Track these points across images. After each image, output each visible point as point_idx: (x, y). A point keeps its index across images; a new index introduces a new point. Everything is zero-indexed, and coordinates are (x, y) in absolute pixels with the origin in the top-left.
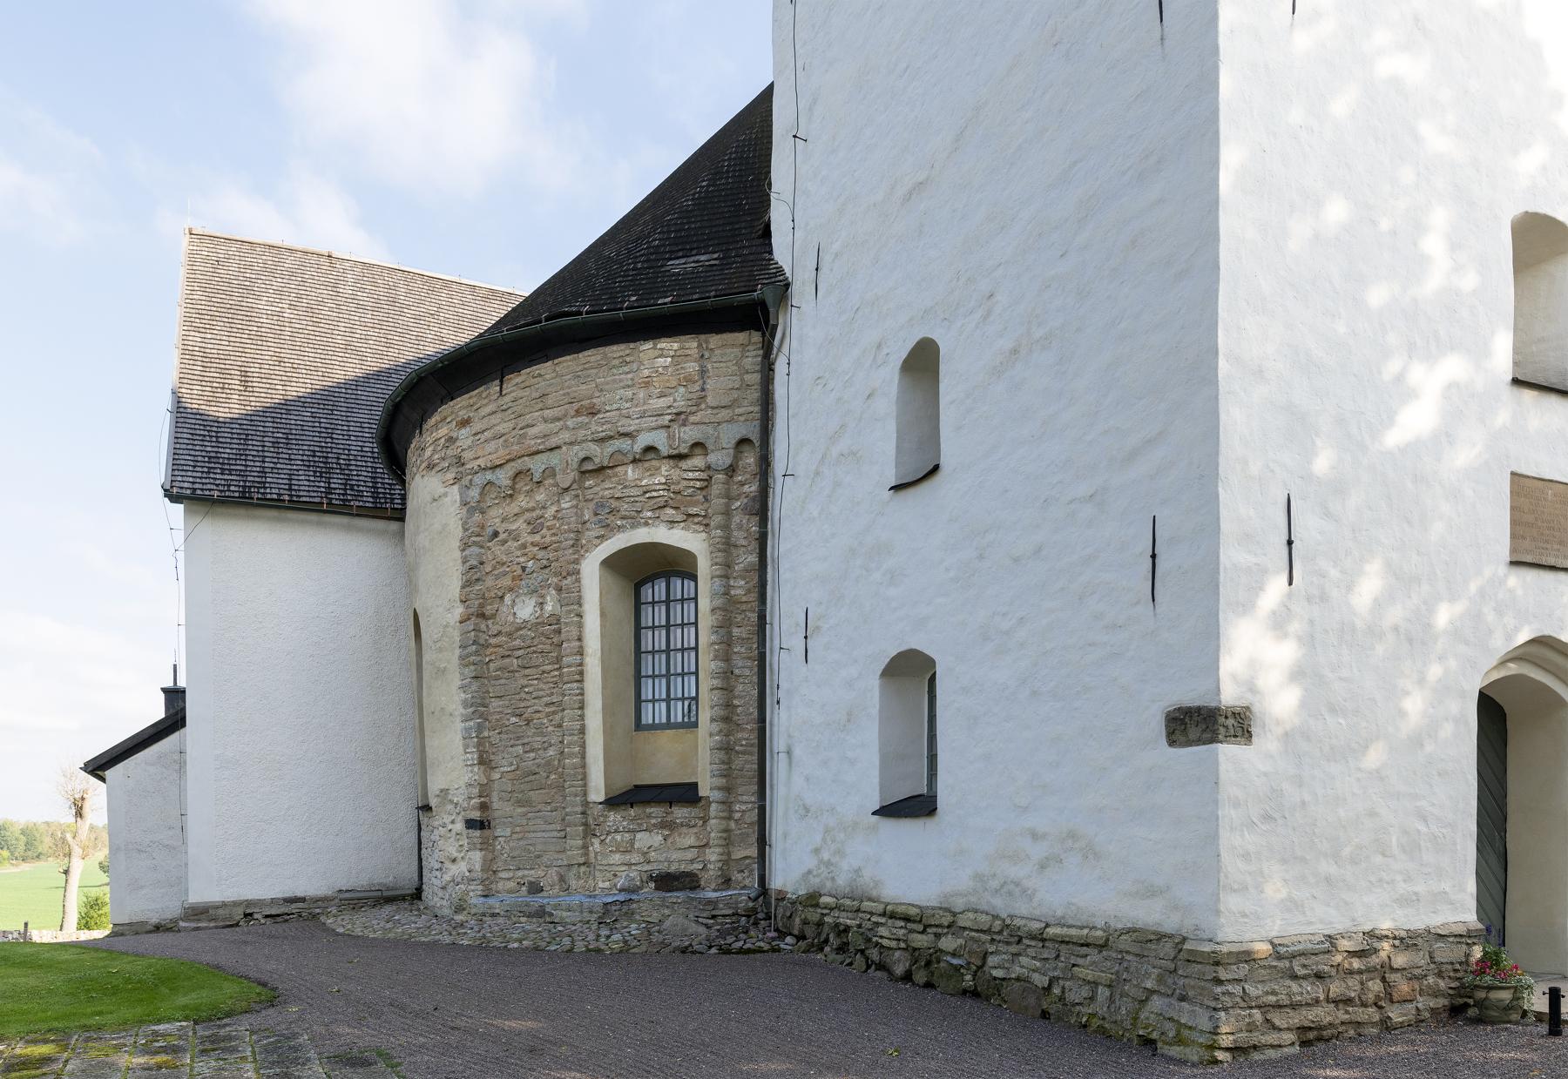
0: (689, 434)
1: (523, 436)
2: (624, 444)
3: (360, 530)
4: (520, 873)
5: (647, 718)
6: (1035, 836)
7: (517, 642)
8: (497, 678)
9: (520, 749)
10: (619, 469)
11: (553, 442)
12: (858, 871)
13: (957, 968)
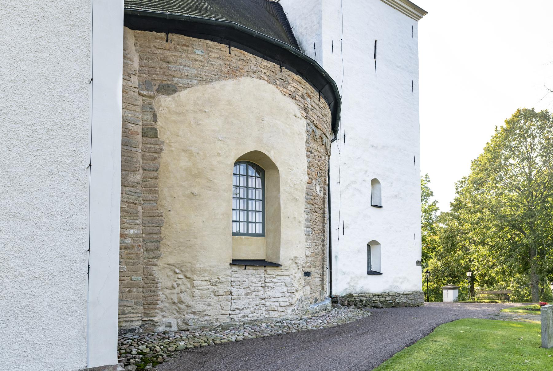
5: (259, 230)
6: (400, 278)
12: (362, 287)
13: (391, 303)
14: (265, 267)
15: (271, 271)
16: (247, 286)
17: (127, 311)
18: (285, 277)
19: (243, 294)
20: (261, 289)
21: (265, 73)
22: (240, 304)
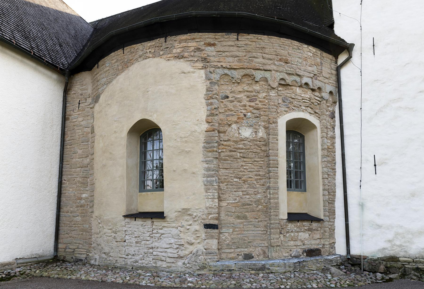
0: (318, 84)
1: (252, 61)
2: (298, 79)
3: (40, 72)
4: (239, 250)
7: (241, 146)
8: (225, 160)
9: (241, 193)
10: (293, 87)
11: (268, 68)
14: (152, 219)
15: (158, 223)
16: (137, 236)
17: (80, 247)
18: (171, 229)
19: (134, 242)
20: (148, 238)
21: (150, 52)
22: (131, 250)
